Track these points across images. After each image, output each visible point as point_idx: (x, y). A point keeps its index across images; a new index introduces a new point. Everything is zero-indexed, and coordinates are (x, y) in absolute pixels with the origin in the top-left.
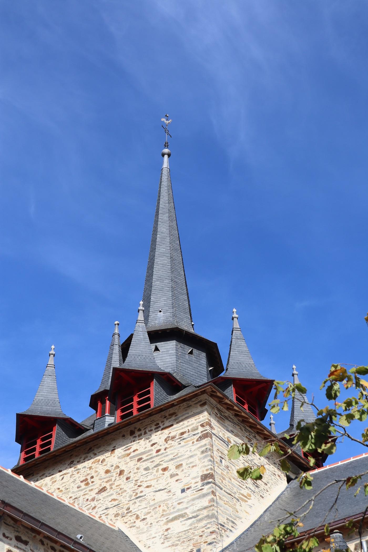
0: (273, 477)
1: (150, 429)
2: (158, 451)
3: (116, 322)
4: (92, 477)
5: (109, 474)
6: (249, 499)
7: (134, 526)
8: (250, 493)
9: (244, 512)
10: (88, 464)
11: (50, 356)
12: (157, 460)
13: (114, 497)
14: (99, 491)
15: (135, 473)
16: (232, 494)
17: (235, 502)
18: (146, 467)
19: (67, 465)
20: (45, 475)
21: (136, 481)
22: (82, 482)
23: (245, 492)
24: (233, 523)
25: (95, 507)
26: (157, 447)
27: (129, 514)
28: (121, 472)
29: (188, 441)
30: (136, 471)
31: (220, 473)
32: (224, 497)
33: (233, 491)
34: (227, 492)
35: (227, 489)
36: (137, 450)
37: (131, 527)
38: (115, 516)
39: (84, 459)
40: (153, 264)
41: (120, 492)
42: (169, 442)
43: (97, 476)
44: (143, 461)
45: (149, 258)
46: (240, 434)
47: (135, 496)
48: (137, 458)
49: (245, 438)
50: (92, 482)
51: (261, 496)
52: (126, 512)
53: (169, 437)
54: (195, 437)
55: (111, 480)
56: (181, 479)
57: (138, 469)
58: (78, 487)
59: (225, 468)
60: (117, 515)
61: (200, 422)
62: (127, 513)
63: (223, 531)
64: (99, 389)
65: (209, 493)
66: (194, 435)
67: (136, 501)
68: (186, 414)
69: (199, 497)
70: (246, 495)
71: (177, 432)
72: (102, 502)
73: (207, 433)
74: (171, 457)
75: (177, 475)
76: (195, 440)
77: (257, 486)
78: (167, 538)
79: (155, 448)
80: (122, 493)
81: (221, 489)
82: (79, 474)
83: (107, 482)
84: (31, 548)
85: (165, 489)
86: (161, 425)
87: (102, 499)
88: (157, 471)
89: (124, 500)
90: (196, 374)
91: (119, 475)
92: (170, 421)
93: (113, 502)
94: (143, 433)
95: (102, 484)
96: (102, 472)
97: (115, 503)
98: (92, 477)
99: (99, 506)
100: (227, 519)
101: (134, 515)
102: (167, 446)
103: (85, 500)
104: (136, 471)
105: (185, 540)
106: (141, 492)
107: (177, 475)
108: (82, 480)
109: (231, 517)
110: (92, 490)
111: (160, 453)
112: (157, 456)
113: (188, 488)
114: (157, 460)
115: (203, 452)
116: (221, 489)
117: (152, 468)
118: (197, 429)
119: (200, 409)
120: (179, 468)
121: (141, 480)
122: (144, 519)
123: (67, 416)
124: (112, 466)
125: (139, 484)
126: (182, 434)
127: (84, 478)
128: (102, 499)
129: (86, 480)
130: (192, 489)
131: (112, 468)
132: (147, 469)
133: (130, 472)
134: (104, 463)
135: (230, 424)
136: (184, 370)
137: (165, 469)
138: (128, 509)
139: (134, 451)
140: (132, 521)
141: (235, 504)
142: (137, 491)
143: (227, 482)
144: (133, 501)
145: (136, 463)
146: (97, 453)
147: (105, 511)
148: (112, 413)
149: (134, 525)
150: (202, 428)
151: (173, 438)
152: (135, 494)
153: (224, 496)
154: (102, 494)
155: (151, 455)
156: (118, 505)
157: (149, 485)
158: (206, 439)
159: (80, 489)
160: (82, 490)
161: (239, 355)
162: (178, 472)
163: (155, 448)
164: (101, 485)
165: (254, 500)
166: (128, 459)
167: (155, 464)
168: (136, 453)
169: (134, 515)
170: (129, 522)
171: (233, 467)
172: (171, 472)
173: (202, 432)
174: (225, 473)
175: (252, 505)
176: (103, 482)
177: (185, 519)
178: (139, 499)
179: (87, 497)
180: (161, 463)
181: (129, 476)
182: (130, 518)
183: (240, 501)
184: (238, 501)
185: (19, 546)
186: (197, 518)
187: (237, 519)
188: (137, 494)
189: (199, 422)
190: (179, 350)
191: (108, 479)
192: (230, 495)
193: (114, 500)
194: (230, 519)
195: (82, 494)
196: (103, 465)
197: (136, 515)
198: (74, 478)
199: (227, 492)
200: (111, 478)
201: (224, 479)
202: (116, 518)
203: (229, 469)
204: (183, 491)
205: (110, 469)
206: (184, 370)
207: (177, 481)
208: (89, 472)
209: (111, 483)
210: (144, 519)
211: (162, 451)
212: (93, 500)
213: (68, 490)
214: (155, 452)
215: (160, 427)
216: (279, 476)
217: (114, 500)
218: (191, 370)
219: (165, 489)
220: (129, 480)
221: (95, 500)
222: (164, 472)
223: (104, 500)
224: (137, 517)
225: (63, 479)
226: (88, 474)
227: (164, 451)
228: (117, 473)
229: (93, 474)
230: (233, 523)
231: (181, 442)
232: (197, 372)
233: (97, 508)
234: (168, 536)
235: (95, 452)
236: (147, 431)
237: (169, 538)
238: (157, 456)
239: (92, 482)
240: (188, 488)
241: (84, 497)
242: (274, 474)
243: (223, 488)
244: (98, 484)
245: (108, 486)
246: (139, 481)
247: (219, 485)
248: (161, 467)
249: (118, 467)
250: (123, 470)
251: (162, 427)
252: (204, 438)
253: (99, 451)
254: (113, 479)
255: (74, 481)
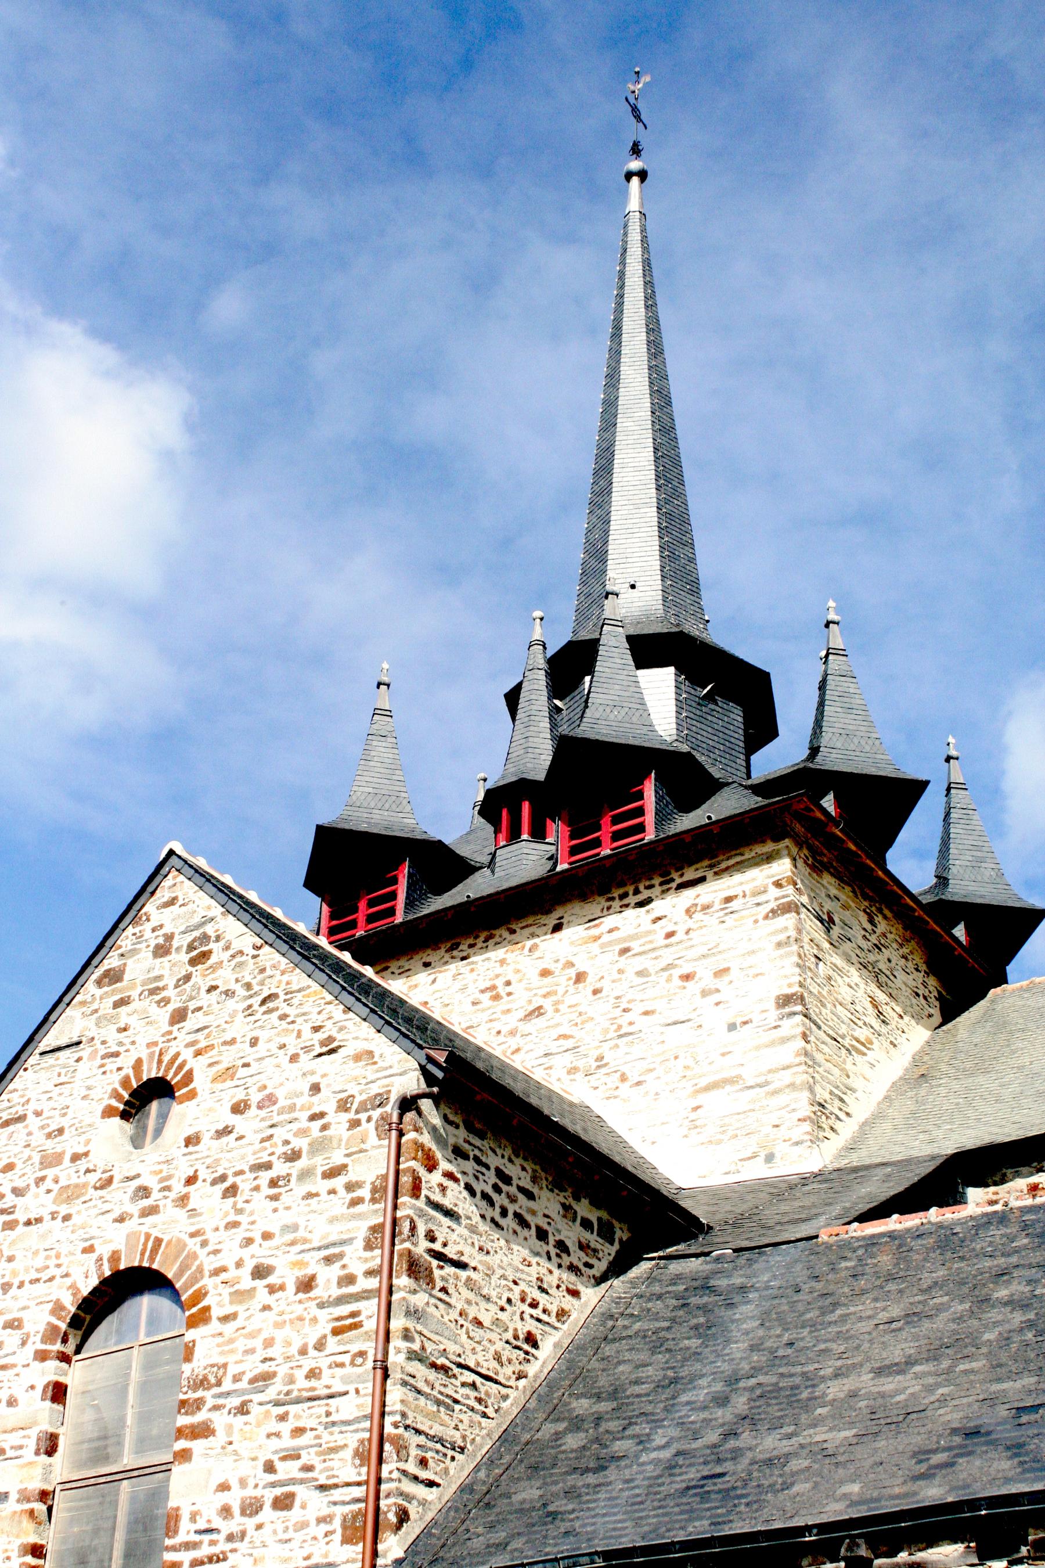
0: (914, 1001)
1: (647, 883)
2: (670, 935)
3: (538, 614)
4: (508, 983)
5: (548, 980)
6: (869, 1049)
7: (615, 1097)
8: (871, 1036)
9: (861, 1078)
10: (496, 954)
11: (378, 687)
12: (668, 956)
13: (564, 1030)
14: (526, 1016)
15: (614, 981)
16: (839, 1039)
17: (844, 1056)
18: (640, 969)
19: (443, 950)
20: (390, 970)
21: (617, 998)
22: (482, 991)
23: (863, 1033)
24: (841, 1100)
25: (518, 1050)
26: (665, 926)
27: (604, 1070)
28: (580, 978)
29: (742, 918)
30: (617, 976)
31: (815, 991)
32: (823, 1046)
33: (840, 1033)
34: (829, 1035)
35: (830, 1027)
36: (617, 929)
37: (608, 1098)
38: (569, 1073)
39: (486, 941)
40: (611, 461)
41: (579, 1020)
42: (698, 916)
43: (521, 981)
44: (634, 955)
45: (599, 446)
46: (853, 905)
47: (616, 1031)
48: (617, 948)
49: (862, 914)
50: (509, 994)
51: (892, 1043)
52: (595, 1064)
53: (696, 905)
54: (760, 908)
55: (555, 993)
56: (727, 1002)
57: (620, 971)
58: (474, 1004)
59: (824, 982)
60: (573, 1070)
61: (773, 876)
62: (599, 1067)
63: (824, 1117)
64: (503, 777)
65: (794, 1037)
66: (758, 904)
67: (620, 1042)
68: (736, 855)
69: (772, 1044)
70: (863, 1040)
71: (714, 895)
72: (537, 1040)
73: (789, 903)
74: (704, 950)
75: (718, 991)
76: (760, 917)
77: (883, 1022)
78: (696, 1127)
79: (662, 928)
80: (583, 1023)
81: (819, 1028)
82: (475, 973)
83: (545, 996)
84: (492, 1145)
85: (688, 1021)
86: (675, 875)
87: (535, 1034)
88: (669, 980)
89: (589, 1038)
90: (722, 747)
91: (575, 983)
92: (697, 869)
93: (561, 1042)
94: (631, 893)
95: (534, 999)
96: (533, 974)
97: (569, 1043)
98: (508, 983)
99: (526, 1048)
100: (831, 1093)
101: (616, 1072)
102: (690, 923)
103: (494, 1032)
104: (617, 976)
105: (739, 1132)
106: (631, 1024)
107: (718, 991)
108: (483, 988)
109: (837, 1087)
110: (509, 1011)
111: (672, 940)
112: (667, 946)
113: (745, 1023)
114: (668, 956)
115: (779, 945)
116: (819, 1028)
117: (657, 972)
118: (765, 892)
119: (769, 847)
120: (721, 976)
121: (629, 997)
122: (639, 1083)
123: (432, 835)
124: (557, 961)
125: (624, 1005)
126: (728, 900)
127: (488, 984)
128: (535, 1034)
129: (494, 987)
130: (755, 1024)
131: (556, 965)
132: (640, 974)
133: (602, 977)
134: (537, 954)
135: (833, 880)
136: (695, 735)
137: (687, 977)
138: (600, 1058)
139: (610, 931)
140: (610, 1085)
141: (844, 1062)
142: (619, 1021)
143: (828, 1012)
144: (612, 1043)
145: (617, 958)
146: (518, 930)
147: (544, 1060)
148: (539, 834)
149: (616, 1093)
150: (778, 890)
151: (706, 908)
152: (615, 1027)
153: (823, 1043)
154: (533, 1021)
155: (651, 942)
156: (575, 1048)
157: (649, 1009)
158: (787, 916)
159: (478, 1007)
160: (483, 1010)
161: (843, 715)
162: (720, 983)
163: (662, 928)
164: (530, 1002)
165: (877, 1051)
166: (595, 947)
167: (663, 963)
168: (615, 935)
169: (616, 1072)
170: (602, 1088)
171: (838, 978)
172: (702, 985)
173: (776, 899)
174: (824, 993)
175: (875, 1063)
176: (536, 995)
177: (740, 1087)
178: (625, 1039)
179: (497, 1026)
180: (676, 962)
181: (598, 986)
182: (605, 1079)
183: (853, 1053)
184: (850, 1054)
185: (473, 1141)
186: (766, 1088)
187: (849, 1092)
188: (620, 1027)
189: (769, 877)
190: (682, 686)
191: (548, 990)
192: (835, 1040)
193: (565, 1037)
194: (836, 1092)
195: (487, 1019)
196: (534, 957)
197: (619, 1073)
198: (463, 983)
199: (829, 1035)
200: (555, 988)
201: (824, 1005)
202: (572, 1077)
203: (833, 983)
204: (732, 1027)
205: (552, 967)
206: (695, 735)
207: (717, 1004)
208: (499, 970)
209: (554, 998)
210: (639, 1083)
211: (680, 936)
212: (513, 1033)
213: (450, 1007)
214: (663, 936)
215: (673, 880)
216: (925, 998)
217: (565, 1037)
218: (710, 736)
219: (688, 1021)
220: (599, 995)
221: (519, 1035)
222: (685, 984)
223: (540, 1036)
224: (623, 1078)
225: (434, 981)
226: (497, 976)
227: (686, 937)
228: (570, 979)
229: (513, 978)
230: (841, 1100)
231: (726, 918)
232: (722, 741)
233: (522, 1052)
234: (697, 1123)
235: (514, 926)
236: (641, 887)
237: (701, 1127)
238: (667, 946)
239: (509, 994)
240: (745, 1023)
241: (490, 1025)
242: (918, 995)
243: (823, 1027)
244: (521, 1000)
245: (547, 1004)
246: (624, 1000)
247: (816, 1018)
248: (676, 973)
249: (572, 965)
250: (585, 973)
251: (678, 881)
252: (783, 913)
253: (521, 925)
254: (561, 990)
255: (464, 989)
